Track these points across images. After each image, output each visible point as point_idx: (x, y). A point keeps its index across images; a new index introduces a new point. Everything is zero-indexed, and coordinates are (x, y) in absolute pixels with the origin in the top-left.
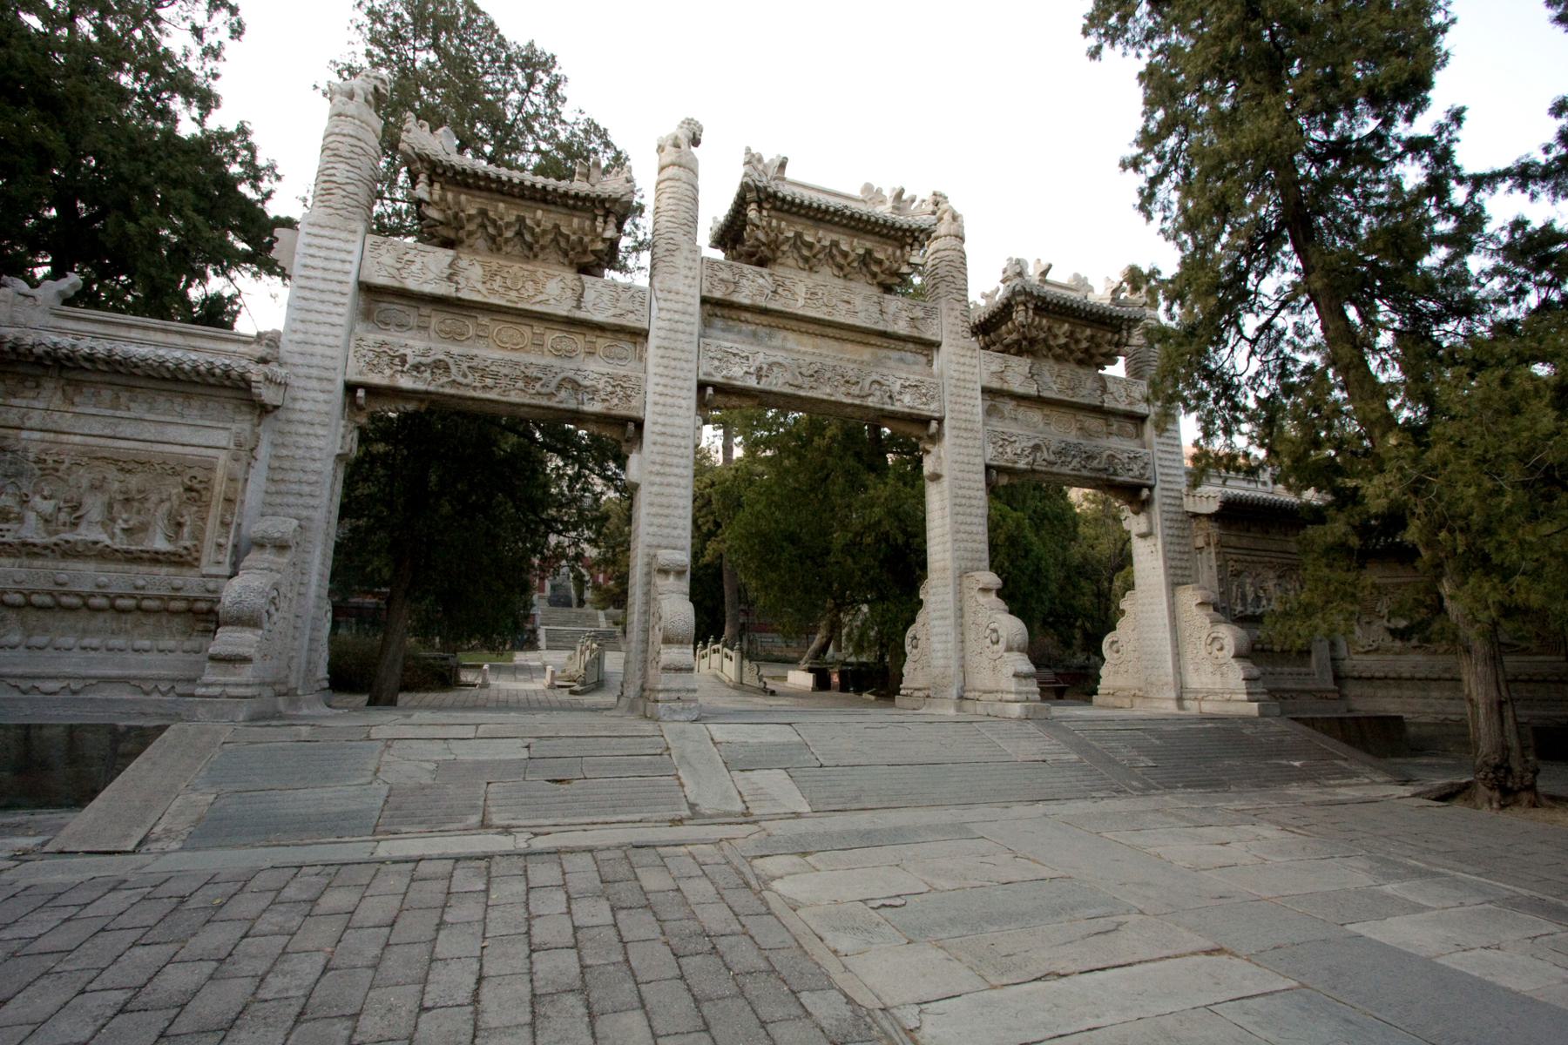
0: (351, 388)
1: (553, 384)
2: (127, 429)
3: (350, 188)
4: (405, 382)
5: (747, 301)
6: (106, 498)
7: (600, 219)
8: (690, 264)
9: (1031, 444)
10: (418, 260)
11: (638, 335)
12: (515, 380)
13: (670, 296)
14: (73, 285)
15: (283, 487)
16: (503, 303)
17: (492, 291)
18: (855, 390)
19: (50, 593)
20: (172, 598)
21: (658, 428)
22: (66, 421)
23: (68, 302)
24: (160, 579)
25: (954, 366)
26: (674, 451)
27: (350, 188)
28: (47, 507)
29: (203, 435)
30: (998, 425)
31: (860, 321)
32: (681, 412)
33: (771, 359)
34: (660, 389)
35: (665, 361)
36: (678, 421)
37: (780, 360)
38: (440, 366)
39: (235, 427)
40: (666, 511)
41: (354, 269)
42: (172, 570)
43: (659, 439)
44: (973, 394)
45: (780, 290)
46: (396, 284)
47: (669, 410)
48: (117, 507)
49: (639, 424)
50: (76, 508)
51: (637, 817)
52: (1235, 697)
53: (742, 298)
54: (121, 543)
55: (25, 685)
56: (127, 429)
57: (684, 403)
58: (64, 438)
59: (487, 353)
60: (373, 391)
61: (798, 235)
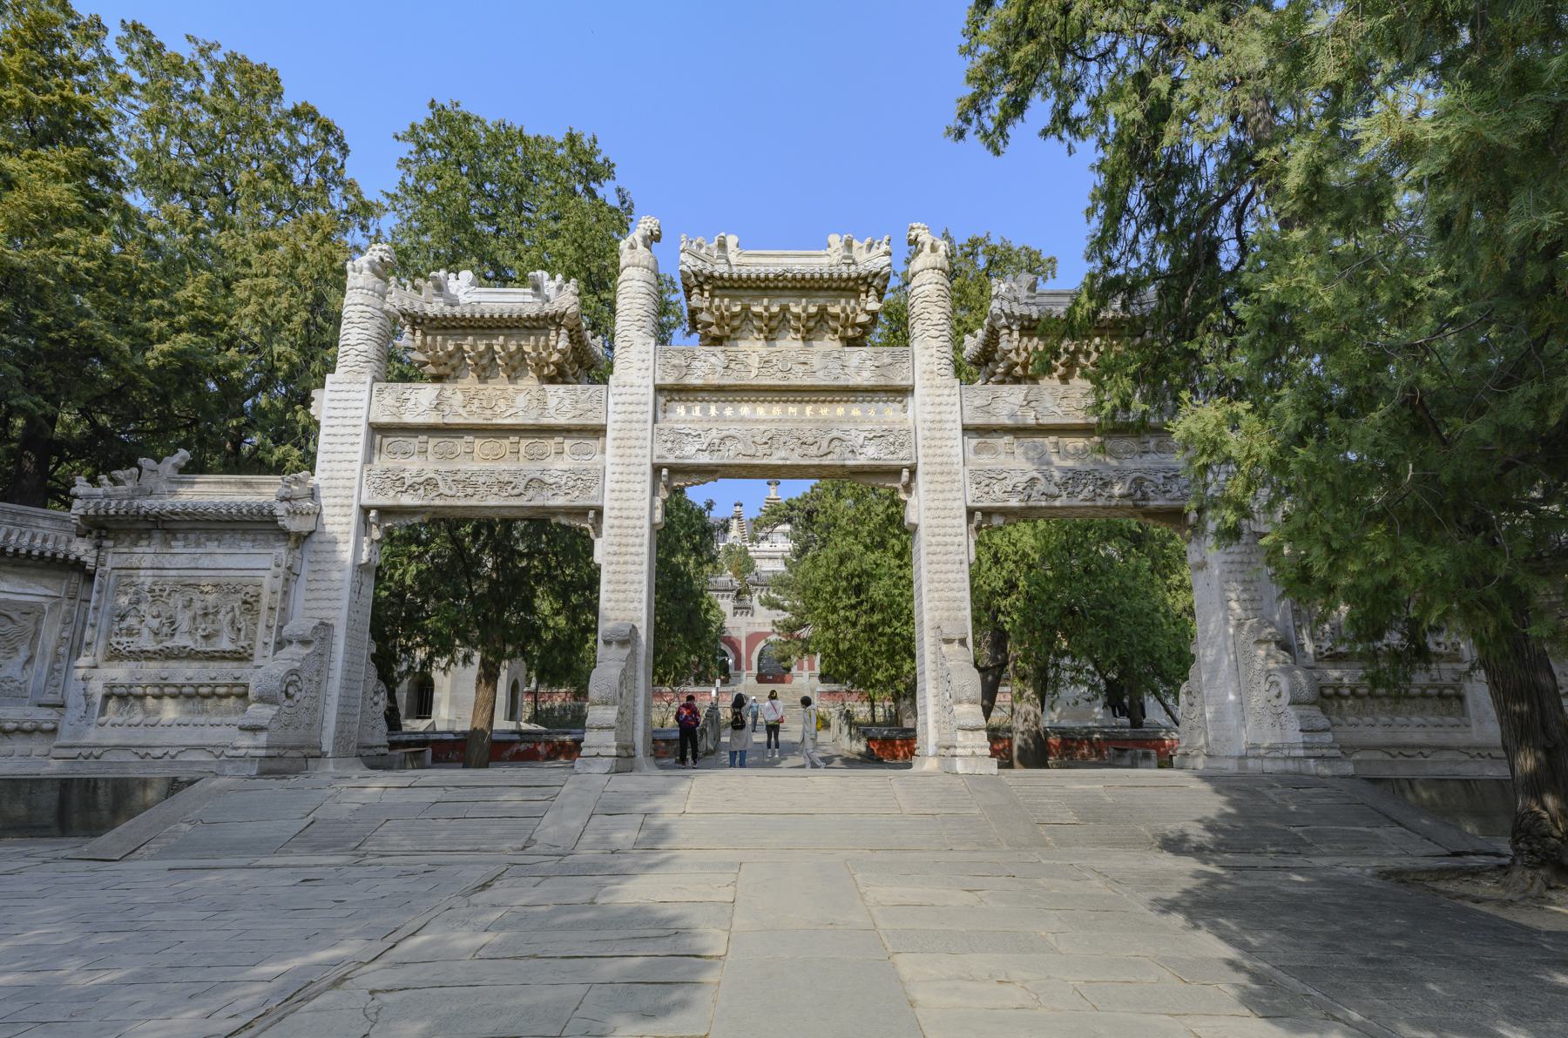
0: (365, 510)
1: (522, 487)
2: (205, 562)
3: (361, 348)
4: (407, 500)
5: (699, 382)
6: (191, 614)
7: (553, 333)
8: (644, 356)
9: (1026, 478)
10: (412, 397)
11: (598, 431)
12: (491, 486)
13: (624, 390)
14: (183, 458)
15: (316, 594)
16: (480, 421)
17: (471, 413)
18: (813, 450)
19: (157, 685)
20: (235, 685)
21: (615, 513)
22: (166, 561)
23: (182, 471)
24: (224, 672)
25: (930, 408)
26: (630, 531)
27: (361, 348)
28: (155, 623)
29: (257, 563)
30: (986, 460)
31: (821, 380)
32: (635, 495)
33: (725, 433)
34: (617, 477)
35: (621, 451)
36: (633, 504)
37: (732, 432)
38: (429, 483)
39: (275, 552)
40: (623, 587)
41: (363, 413)
42: (235, 664)
43: (616, 522)
44: (952, 434)
45: (732, 365)
46: (396, 420)
47: (624, 495)
48: (199, 619)
49: (599, 512)
50: (172, 623)
51: (244, 862)
52: (1293, 753)
53: (692, 380)
54: (202, 646)
55: (142, 752)
56: (205, 562)
57: (639, 487)
58: (165, 573)
59: (465, 466)
60: (384, 512)
61: (746, 309)
